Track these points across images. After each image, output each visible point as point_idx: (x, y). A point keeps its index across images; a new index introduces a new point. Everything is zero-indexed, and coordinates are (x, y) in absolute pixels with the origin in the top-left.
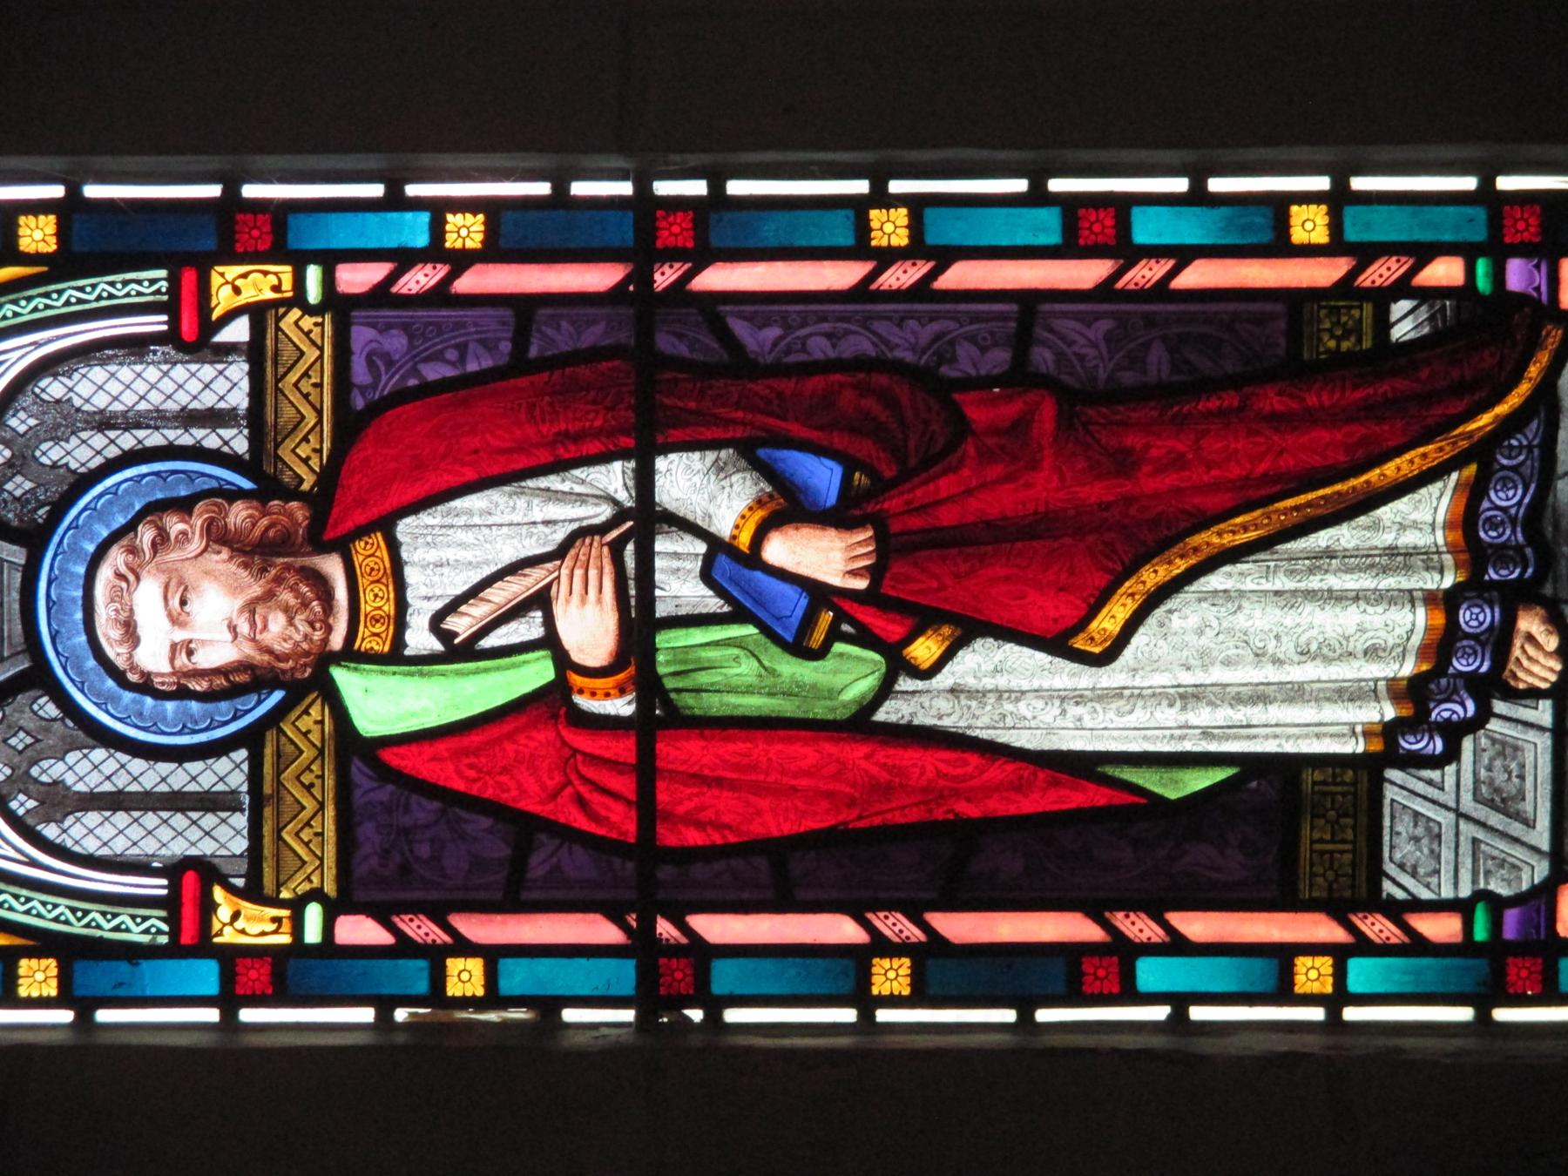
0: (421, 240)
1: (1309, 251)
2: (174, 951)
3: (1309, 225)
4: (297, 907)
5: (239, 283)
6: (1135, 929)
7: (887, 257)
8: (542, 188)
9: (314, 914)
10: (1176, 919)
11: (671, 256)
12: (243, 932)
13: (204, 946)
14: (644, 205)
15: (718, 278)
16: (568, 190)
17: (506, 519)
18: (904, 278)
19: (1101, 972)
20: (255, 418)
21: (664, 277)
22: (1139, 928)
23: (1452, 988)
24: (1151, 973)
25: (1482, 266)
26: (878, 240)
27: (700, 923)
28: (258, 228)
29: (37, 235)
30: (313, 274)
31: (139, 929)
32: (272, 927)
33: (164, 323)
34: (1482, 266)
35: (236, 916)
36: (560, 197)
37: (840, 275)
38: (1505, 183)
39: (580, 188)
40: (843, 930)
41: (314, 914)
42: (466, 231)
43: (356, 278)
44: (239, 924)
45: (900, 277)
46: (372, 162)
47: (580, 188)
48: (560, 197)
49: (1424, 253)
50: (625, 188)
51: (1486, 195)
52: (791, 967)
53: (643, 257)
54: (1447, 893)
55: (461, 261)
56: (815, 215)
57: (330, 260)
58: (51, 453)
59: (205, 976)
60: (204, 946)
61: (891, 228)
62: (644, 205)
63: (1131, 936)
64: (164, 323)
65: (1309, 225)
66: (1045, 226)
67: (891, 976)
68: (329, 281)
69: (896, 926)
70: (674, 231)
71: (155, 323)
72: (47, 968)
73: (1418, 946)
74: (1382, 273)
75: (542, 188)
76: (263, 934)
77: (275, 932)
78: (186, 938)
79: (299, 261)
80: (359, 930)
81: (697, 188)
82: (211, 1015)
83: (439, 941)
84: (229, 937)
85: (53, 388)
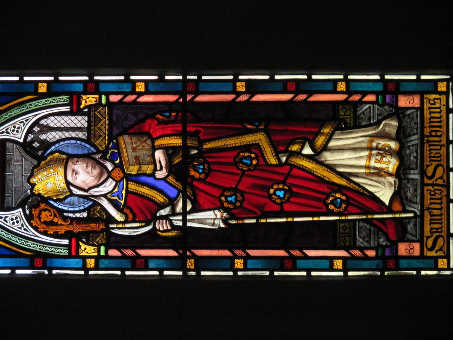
0: (129, 90)
1: (342, 92)
2: (70, 256)
3: (342, 87)
4: (99, 247)
5: (87, 100)
6: (295, 253)
7: (239, 94)
8: (17, 79)
9: (102, 249)
10: (248, 251)
11: (190, 93)
12: (87, 253)
13: (77, 256)
14: (185, 81)
15: (201, 98)
16: (384, 77)
17: (427, 154)
18: (130, 97)
19: (289, 264)
20: (88, 129)
21: (189, 97)
22: (296, 253)
23: (171, 267)
24: (300, 263)
25: (380, 97)
26: (138, 90)
27: (248, 251)
28: (240, 87)
29: (43, 88)
30: (104, 98)
31: (65, 252)
32: (94, 251)
33: (69, 108)
34: (380, 97)
35: (85, 249)
36: (21, 81)
37: (230, 97)
38: (387, 77)
39: (314, 77)
40: (226, 253)
41: (102, 249)
42: (140, 88)
43: (114, 98)
44: (86, 251)
45: (244, 98)
46: (15, 72)
47: (314, 77)
48: (21, 81)
49: (365, 93)
50: (181, 77)
51: (382, 79)
52: (161, 261)
53: (183, 94)
54: (372, 245)
55: (140, 94)
56: (210, 84)
57: (107, 94)
58: (43, 137)
59: (77, 262)
60: (77, 256)
61: (241, 87)
62: (185, 81)
63: (294, 254)
64: (69, 108)
65: (342, 87)
66: (103, 88)
67: (239, 264)
68: (108, 99)
69: (239, 252)
70: (191, 87)
71: (67, 109)
72: (237, 262)
73: (366, 258)
74: (356, 98)
75: (17, 79)
76: (92, 253)
77: (94, 252)
78: (73, 253)
79: (100, 94)
80: (113, 252)
81: (195, 77)
82: (341, 274)
83: (243, 255)
84: (84, 254)
85: (43, 122)
